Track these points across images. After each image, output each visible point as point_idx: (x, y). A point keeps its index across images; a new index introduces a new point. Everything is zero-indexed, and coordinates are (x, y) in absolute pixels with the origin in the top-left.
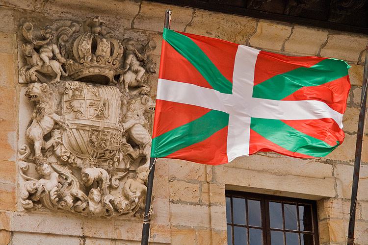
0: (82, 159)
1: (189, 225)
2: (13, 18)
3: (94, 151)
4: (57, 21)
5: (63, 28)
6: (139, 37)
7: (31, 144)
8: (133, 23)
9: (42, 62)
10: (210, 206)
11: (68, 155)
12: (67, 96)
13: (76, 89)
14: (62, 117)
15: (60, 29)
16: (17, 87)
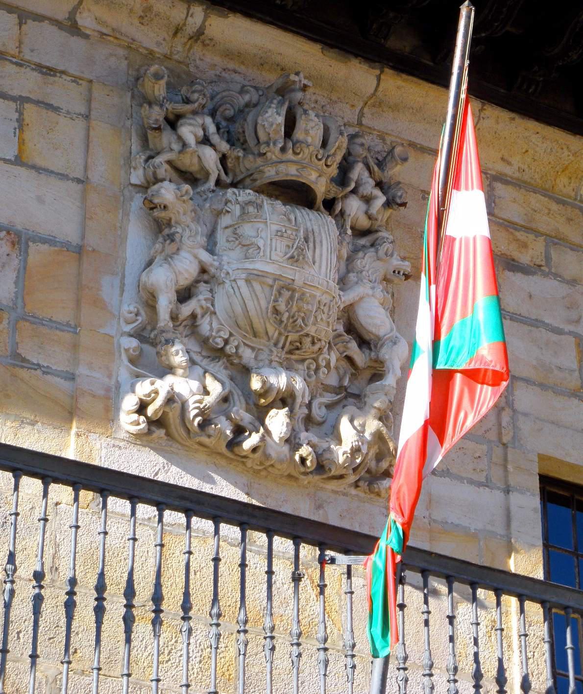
0: (253, 349)
1: (467, 525)
2: (126, 62)
3: (280, 334)
4: (213, 84)
5: (224, 94)
6: (372, 144)
7: (150, 302)
8: (361, 114)
9: (181, 144)
10: (507, 491)
11: (226, 337)
12: (230, 214)
13: (250, 203)
14: (215, 257)
15: (219, 97)
16: (126, 193)
